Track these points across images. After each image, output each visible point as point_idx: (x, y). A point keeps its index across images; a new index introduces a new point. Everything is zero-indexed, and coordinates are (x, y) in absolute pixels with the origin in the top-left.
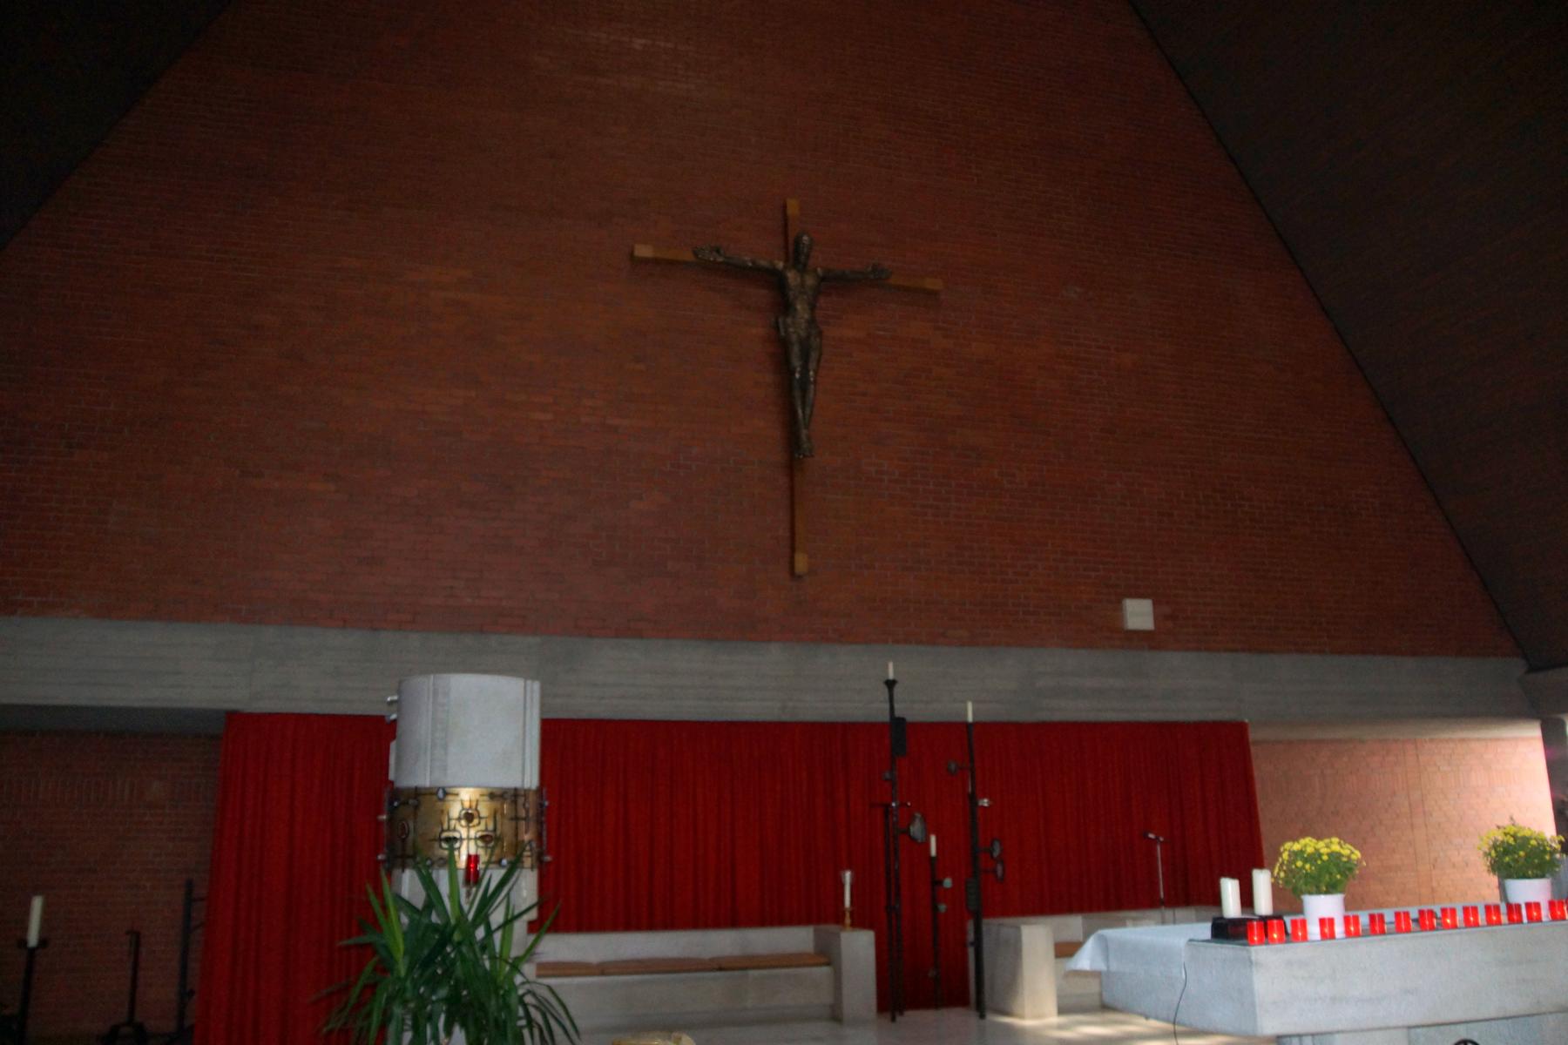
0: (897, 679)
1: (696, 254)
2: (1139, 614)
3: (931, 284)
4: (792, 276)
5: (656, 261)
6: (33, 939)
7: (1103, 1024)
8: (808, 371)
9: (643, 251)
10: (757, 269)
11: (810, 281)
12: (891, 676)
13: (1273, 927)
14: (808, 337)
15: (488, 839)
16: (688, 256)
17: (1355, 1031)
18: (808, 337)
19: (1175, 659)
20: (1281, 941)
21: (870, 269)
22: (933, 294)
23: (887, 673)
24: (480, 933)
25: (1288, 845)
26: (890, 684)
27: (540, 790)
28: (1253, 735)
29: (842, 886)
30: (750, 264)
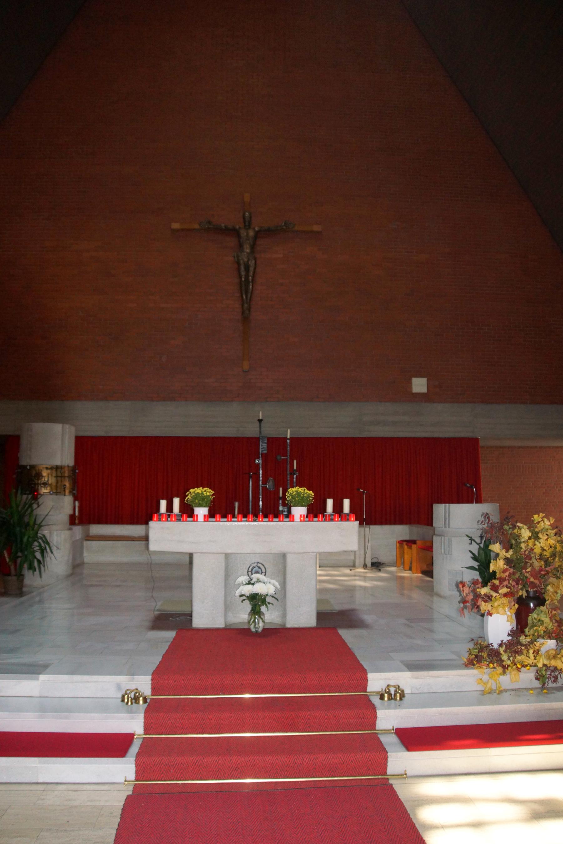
0: (263, 419)
1: (200, 225)
3: (316, 228)
4: (243, 233)
5: (182, 230)
7: (336, 571)
8: (248, 277)
9: (176, 226)
10: (227, 229)
11: (251, 233)
12: (261, 418)
13: (155, 517)
14: (248, 262)
15: (45, 484)
16: (197, 226)
17: (217, 553)
18: (248, 262)
19: (439, 407)
20: (157, 521)
21: (283, 224)
22: (319, 233)
23: (259, 416)
24: (518, 557)
25: (192, 490)
26: (260, 421)
27: (73, 469)
28: (481, 443)
29: (235, 508)
30: (224, 228)
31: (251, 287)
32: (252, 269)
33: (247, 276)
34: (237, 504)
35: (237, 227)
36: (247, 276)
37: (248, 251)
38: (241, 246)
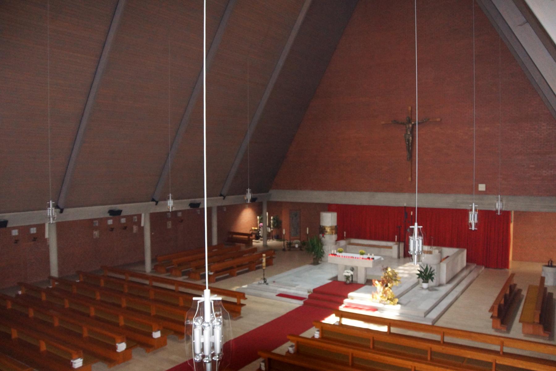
2: (482, 187)
3: (438, 120)
6: (308, 233)
9: (383, 123)
11: (411, 126)
27: (336, 226)
31: (411, 148)
32: (410, 141)
33: (408, 144)
34: (345, 233)
35: (405, 123)
36: (408, 144)
37: (409, 133)
38: (407, 131)
